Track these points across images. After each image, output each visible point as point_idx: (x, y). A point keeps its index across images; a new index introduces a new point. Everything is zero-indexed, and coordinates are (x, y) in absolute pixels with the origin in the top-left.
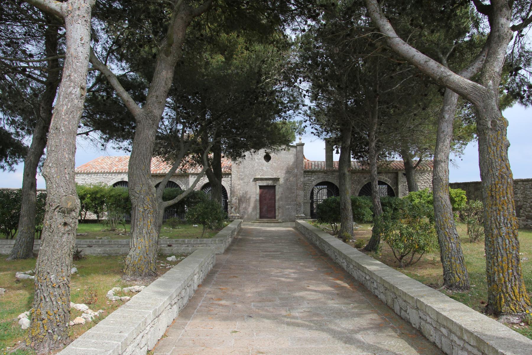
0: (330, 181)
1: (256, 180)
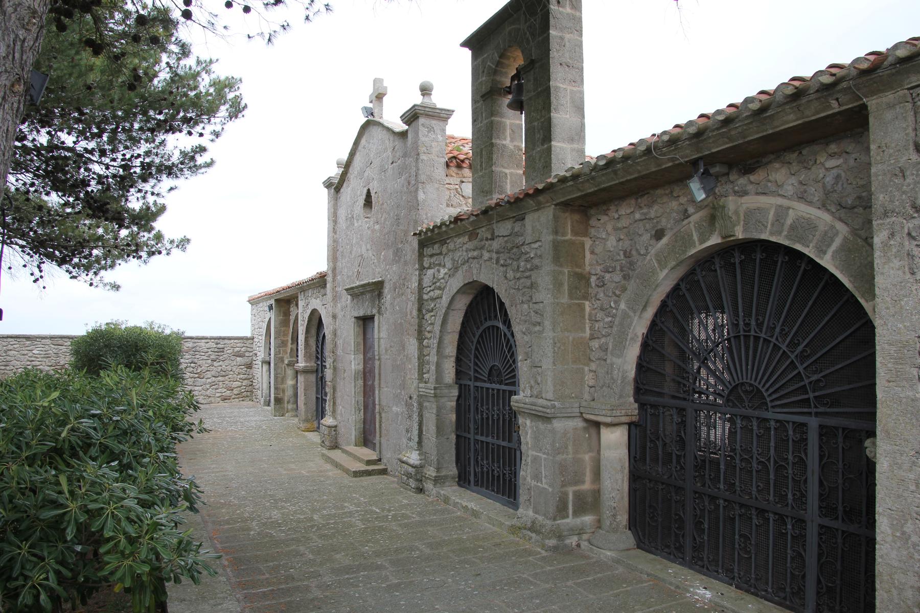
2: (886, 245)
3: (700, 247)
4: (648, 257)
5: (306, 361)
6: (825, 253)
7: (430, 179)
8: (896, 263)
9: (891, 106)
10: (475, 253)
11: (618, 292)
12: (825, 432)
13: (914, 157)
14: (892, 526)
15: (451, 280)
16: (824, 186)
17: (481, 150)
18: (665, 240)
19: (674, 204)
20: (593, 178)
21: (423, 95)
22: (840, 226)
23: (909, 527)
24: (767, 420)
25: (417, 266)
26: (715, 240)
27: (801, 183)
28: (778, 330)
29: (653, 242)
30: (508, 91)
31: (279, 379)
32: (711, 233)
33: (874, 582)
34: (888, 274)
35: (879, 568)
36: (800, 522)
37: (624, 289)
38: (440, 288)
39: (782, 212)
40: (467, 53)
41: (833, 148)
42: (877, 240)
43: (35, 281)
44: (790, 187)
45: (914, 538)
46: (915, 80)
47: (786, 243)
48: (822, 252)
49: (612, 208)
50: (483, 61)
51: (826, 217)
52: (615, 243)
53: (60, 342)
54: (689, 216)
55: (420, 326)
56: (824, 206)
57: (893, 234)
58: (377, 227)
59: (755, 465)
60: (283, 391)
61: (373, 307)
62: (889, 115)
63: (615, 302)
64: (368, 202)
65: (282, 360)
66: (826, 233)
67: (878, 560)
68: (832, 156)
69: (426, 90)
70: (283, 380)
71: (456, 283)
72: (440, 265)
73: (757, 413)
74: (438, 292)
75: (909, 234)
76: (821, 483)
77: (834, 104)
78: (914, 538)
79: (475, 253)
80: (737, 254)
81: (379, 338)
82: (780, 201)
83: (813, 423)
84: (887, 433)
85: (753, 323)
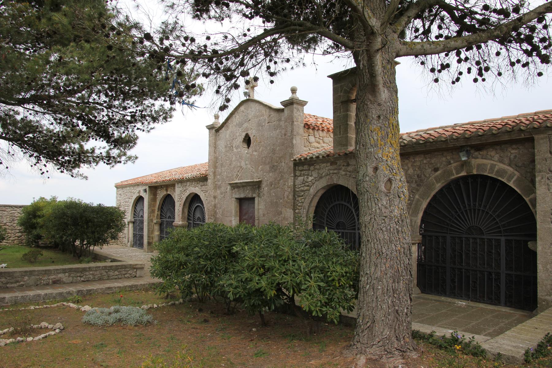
0: (341, 182)
1: (235, 186)
2: (540, 181)
3: (456, 176)
4: (431, 178)
5: (182, 221)
6: (510, 181)
7: (298, 134)
8: (544, 187)
9: (542, 139)
10: (335, 171)
11: (414, 191)
12: (508, 242)
13: (550, 155)
14: (543, 267)
15: (317, 183)
16: (510, 158)
17: (340, 126)
18: (439, 172)
19: (444, 159)
20: (414, 147)
21: (293, 93)
22: (516, 172)
23: (548, 266)
24: (484, 239)
25: (292, 175)
26: (463, 174)
27: (501, 157)
28: (488, 207)
29: (433, 172)
30: (354, 101)
31: (150, 231)
32: (462, 171)
33: (537, 285)
34: (541, 190)
35: (538, 280)
36: (498, 274)
37: (418, 190)
38: (308, 186)
39: (493, 166)
40: (331, 81)
41: (514, 146)
42: (537, 179)
43: (42, 174)
44: (497, 157)
45: (550, 270)
46: (550, 132)
47: (495, 177)
48: (509, 181)
49: (411, 157)
50: (341, 86)
51: (511, 169)
52: (412, 171)
53: (4, 209)
54: (451, 164)
55: (294, 203)
56: (510, 165)
57: (542, 178)
58: (255, 153)
59: (478, 255)
60: (153, 238)
61: (254, 193)
62: (541, 141)
63: (413, 195)
64: (247, 140)
65: (152, 220)
66: (511, 175)
67: (538, 278)
68: (513, 149)
69: (294, 91)
70: (152, 232)
71: (323, 183)
72: (308, 175)
73: (479, 237)
74: (306, 188)
75: (548, 178)
76: (506, 259)
77: (523, 135)
78: (550, 270)
79: (335, 171)
80: (470, 179)
81: (258, 209)
82: (492, 162)
83: (503, 239)
84: (541, 239)
85: (477, 204)
